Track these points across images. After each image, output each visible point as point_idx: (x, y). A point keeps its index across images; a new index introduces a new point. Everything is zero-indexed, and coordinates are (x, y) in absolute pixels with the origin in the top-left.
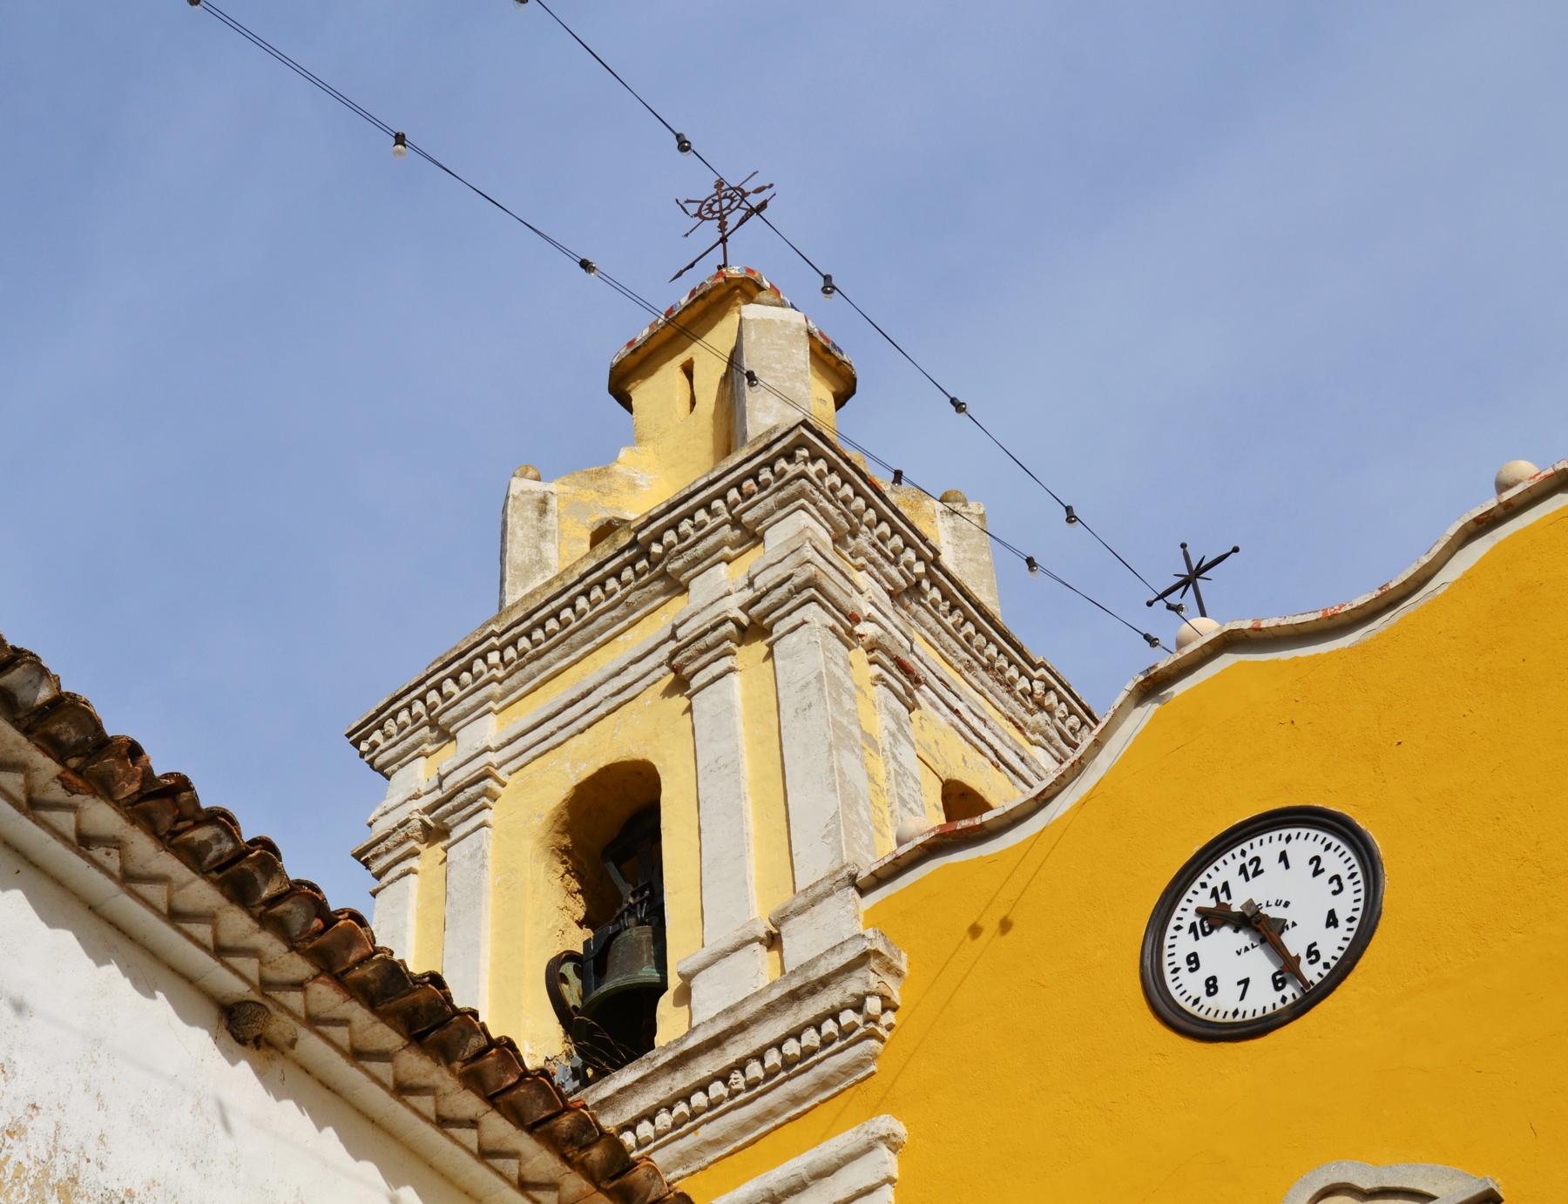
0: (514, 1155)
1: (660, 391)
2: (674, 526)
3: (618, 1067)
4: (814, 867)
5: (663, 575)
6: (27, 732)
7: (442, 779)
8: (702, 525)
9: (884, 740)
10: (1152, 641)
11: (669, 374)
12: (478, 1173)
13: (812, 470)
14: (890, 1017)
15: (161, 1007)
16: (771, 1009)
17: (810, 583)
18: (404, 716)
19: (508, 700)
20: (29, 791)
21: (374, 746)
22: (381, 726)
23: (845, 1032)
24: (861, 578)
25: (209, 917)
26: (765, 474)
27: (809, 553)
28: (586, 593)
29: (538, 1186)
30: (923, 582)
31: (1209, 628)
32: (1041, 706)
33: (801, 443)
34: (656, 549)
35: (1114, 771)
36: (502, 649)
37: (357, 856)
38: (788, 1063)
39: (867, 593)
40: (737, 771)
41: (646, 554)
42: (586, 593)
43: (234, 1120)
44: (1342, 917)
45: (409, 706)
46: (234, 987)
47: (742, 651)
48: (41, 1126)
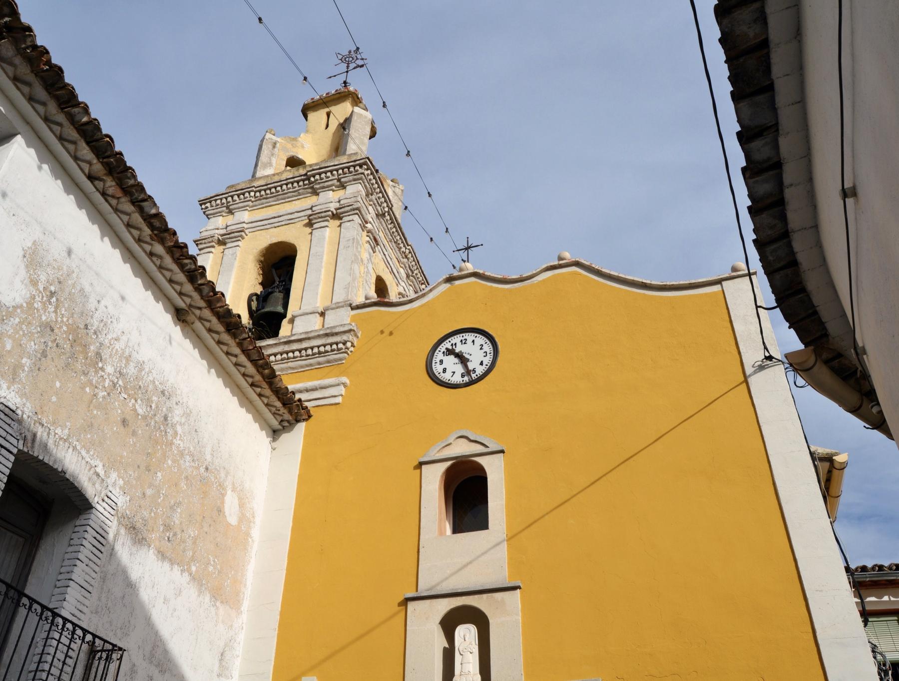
0: (244, 367)
1: (318, 117)
2: (320, 174)
3: (269, 338)
4: (339, 297)
5: (312, 188)
6: (145, 220)
7: (227, 226)
8: (328, 177)
9: (365, 261)
10: (454, 267)
11: (322, 113)
12: (233, 369)
13: (366, 172)
14: (352, 349)
15: (160, 306)
16: (319, 336)
17: (358, 209)
18: (218, 202)
19: (253, 208)
20: (140, 236)
21: (207, 208)
22: (210, 202)
23: (339, 349)
24: (370, 208)
25: (181, 284)
26: (352, 169)
27: (360, 199)
28: (287, 184)
29: (248, 376)
30: (386, 214)
31: (470, 267)
32: (406, 257)
33: (365, 164)
34: (312, 179)
35: (433, 299)
36: (255, 192)
37: (195, 241)
38: (320, 353)
39: (371, 215)
40: (322, 258)
41: (309, 179)
42: (287, 184)
43: (173, 343)
44: (484, 363)
45: (221, 199)
46: (181, 304)
47: (331, 221)
48: (124, 338)
